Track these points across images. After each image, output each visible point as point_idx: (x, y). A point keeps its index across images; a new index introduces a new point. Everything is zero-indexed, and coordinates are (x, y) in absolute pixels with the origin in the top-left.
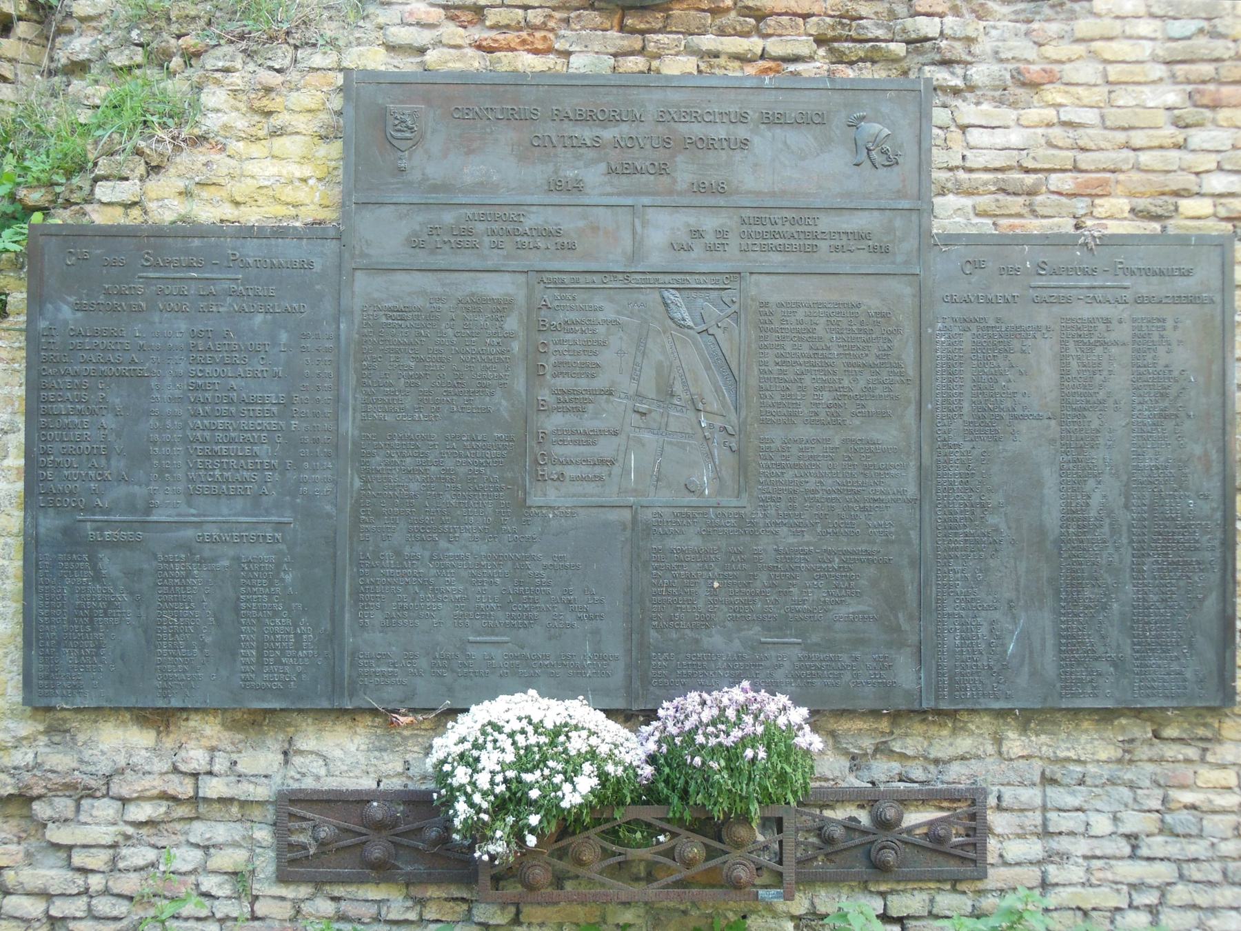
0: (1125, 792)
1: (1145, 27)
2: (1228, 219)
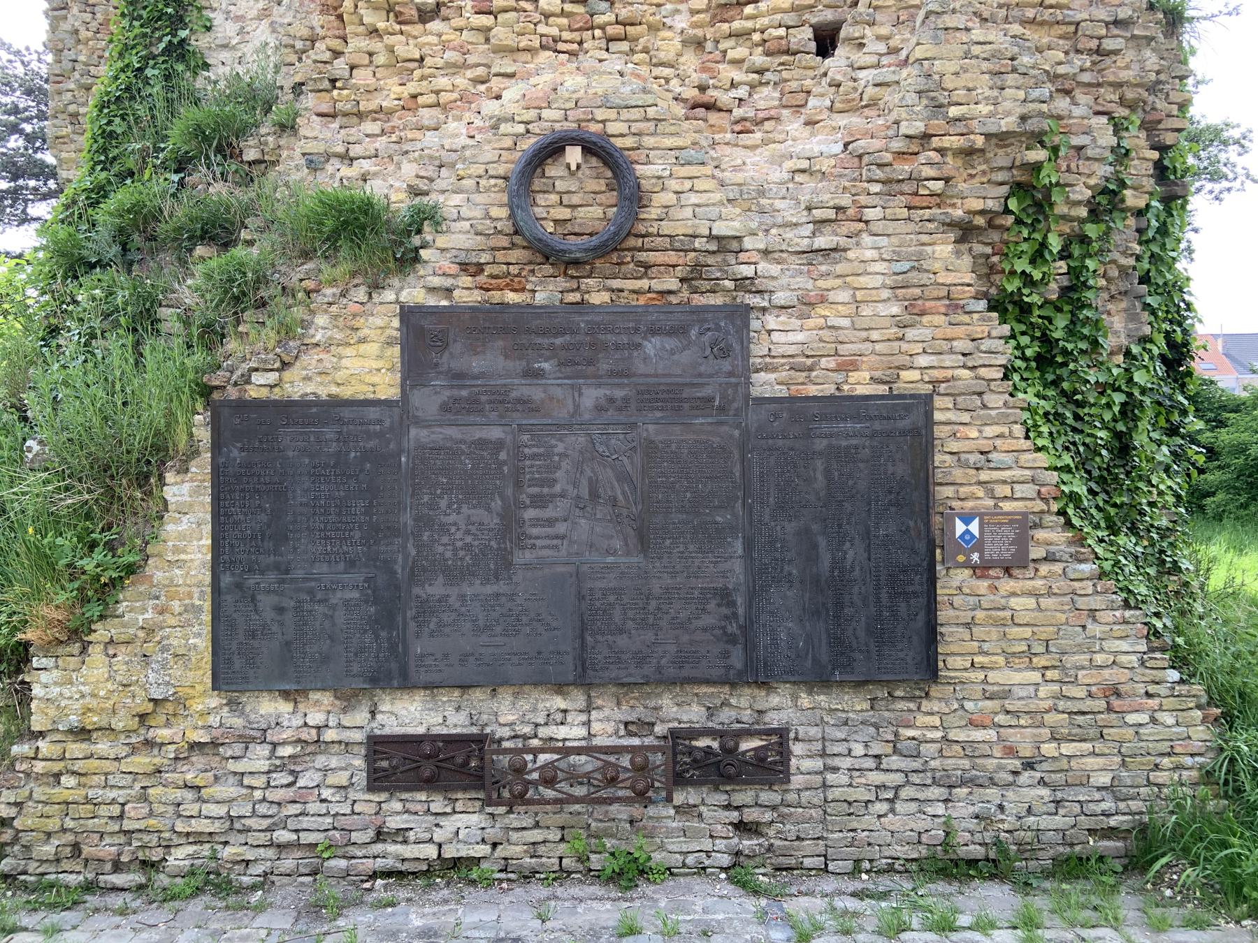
0: (872, 730)
1: (880, 267)
2: (929, 382)
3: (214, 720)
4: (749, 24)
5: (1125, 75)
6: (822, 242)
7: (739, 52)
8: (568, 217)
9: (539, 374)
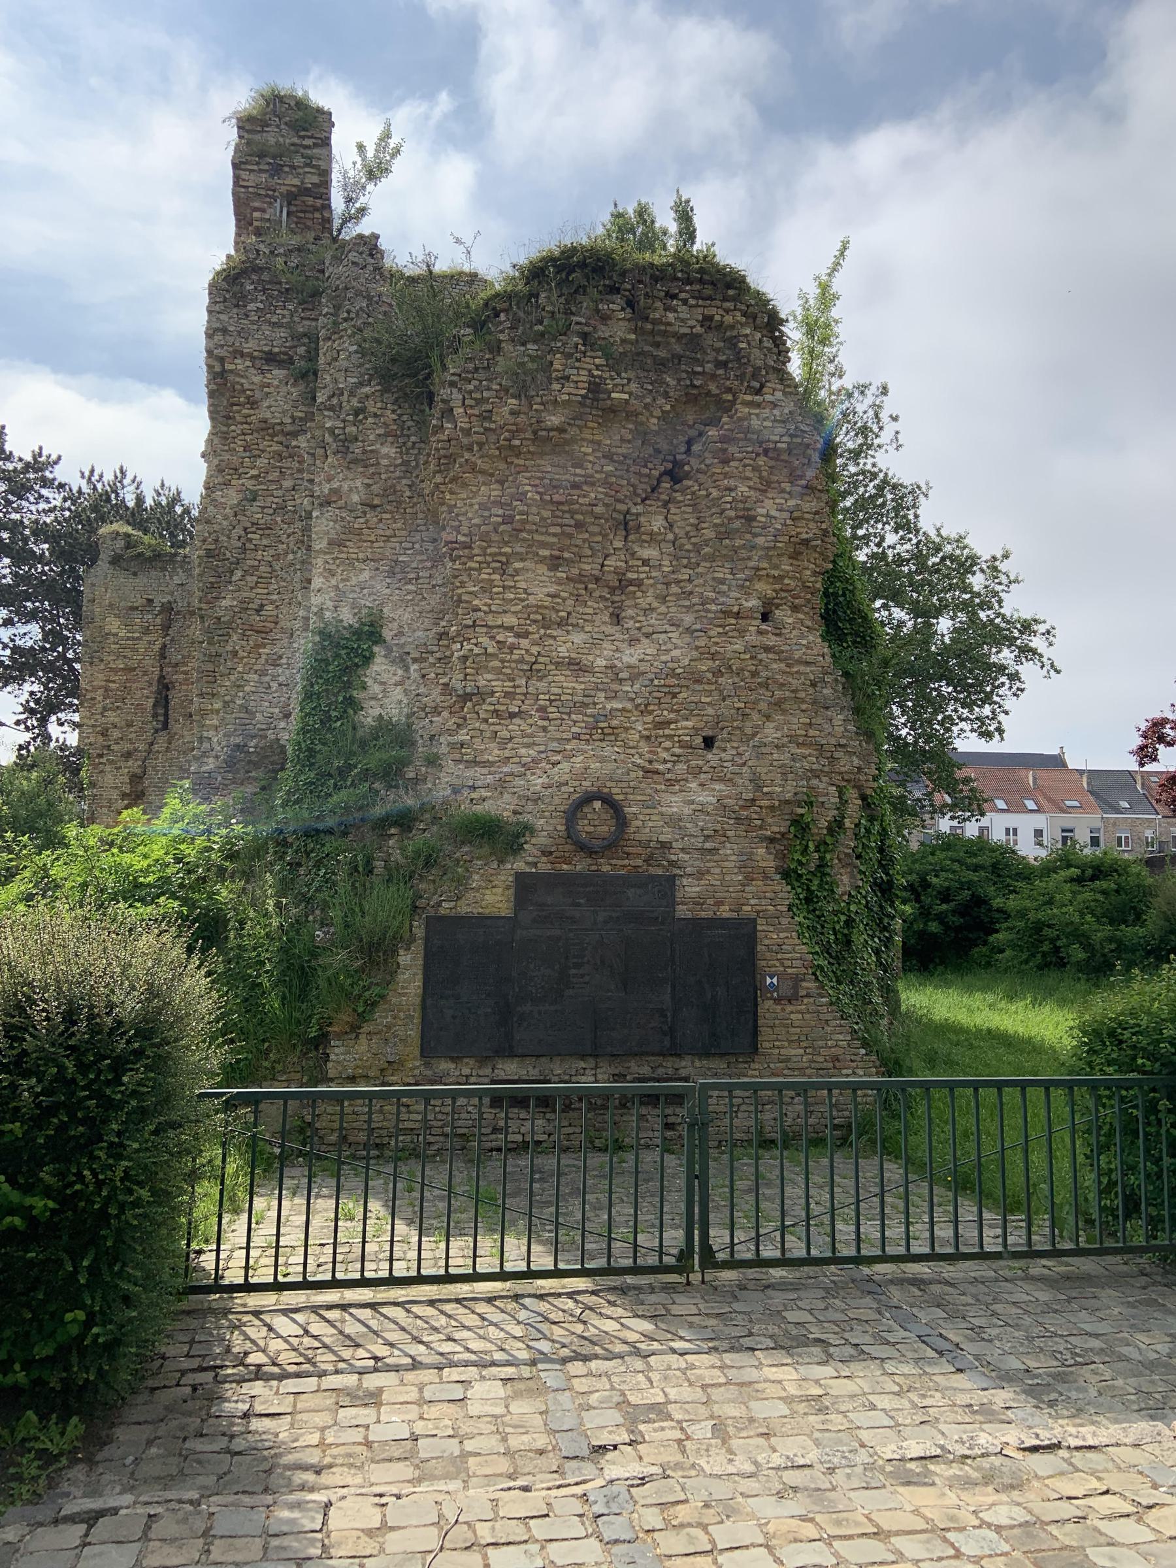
1: (733, 858)
3: (417, 1072)
4: (673, 733)
5: (843, 769)
6: (708, 845)
7: (668, 744)
9: (579, 905)
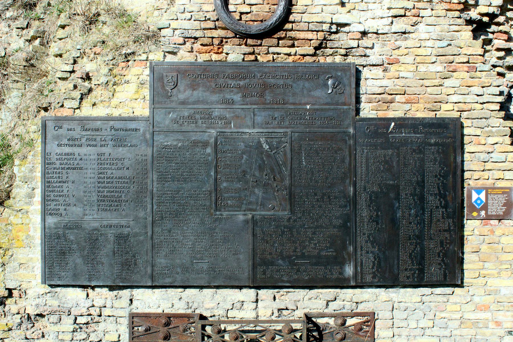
8: (249, 11)
